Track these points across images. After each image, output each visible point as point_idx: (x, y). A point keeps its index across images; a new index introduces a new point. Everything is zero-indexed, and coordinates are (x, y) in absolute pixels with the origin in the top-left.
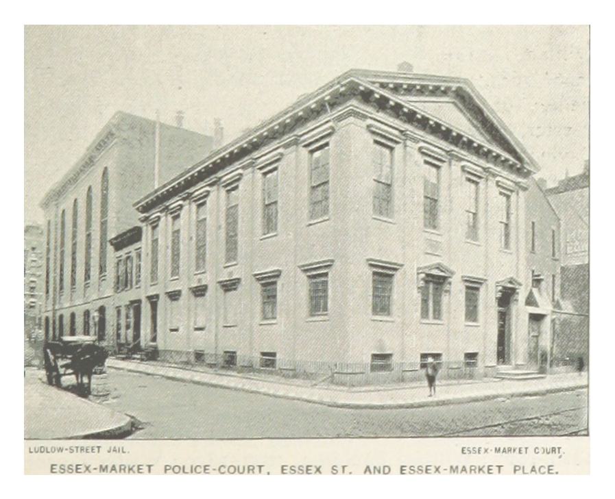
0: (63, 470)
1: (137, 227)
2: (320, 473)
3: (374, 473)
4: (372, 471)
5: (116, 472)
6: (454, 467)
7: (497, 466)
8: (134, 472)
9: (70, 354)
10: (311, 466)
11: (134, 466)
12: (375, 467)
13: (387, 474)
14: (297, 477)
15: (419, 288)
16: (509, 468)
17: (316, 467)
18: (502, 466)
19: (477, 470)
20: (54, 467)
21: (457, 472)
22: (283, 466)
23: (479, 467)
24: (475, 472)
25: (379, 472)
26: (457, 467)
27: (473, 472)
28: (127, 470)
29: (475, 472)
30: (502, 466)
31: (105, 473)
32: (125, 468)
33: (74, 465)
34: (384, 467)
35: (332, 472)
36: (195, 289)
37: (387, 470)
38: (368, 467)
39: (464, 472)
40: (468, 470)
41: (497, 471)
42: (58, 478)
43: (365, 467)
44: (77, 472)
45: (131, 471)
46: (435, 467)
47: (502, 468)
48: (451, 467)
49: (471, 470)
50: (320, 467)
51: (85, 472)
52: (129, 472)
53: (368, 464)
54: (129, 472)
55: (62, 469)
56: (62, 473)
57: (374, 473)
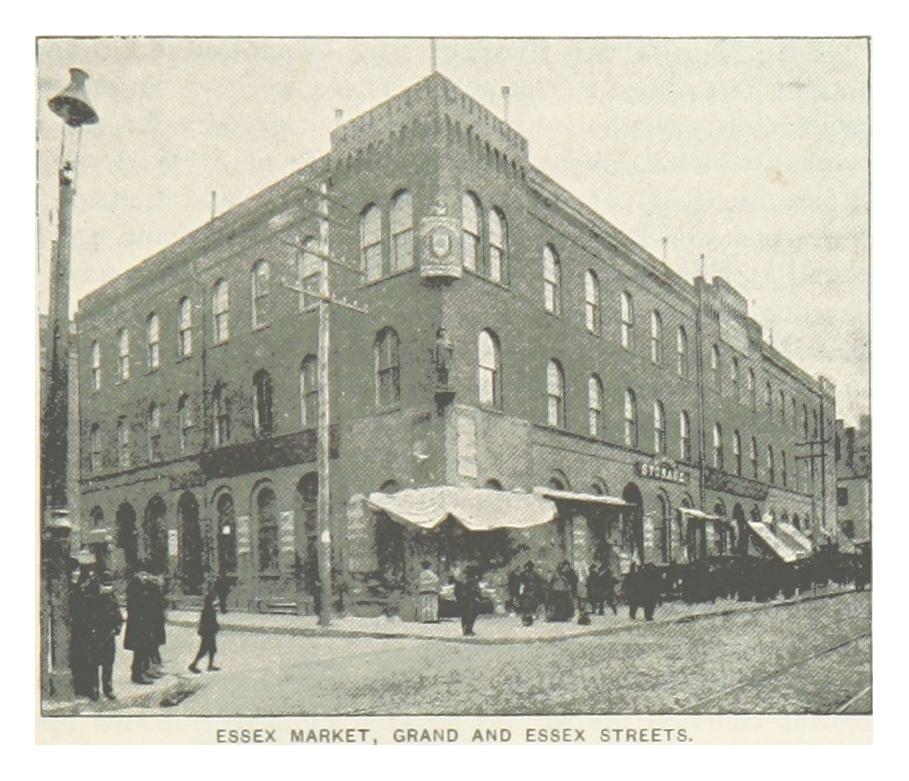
0: (234, 738)
1: (307, 475)
2: (274, 740)
3: (435, 739)
4: (432, 737)
5: (316, 740)
6: (297, 732)
7: (360, 730)
8: (341, 740)
9: (519, 588)
10: (659, 730)
11: (341, 731)
12: (435, 732)
13: (452, 741)
14: (240, 747)
15: (96, 524)
16: (519, 734)
17: (267, 732)
18: (367, 730)
19: (331, 737)
20: (531, 733)
21: (302, 740)
22: (528, 730)
23: (334, 732)
24: (328, 740)
25: (495, 738)
26: (301, 732)
27: (324, 739)
28: (331, 737)
29: (328, 740)
30: (367, 730)
31: (299, 743)
32: (635, 733)
33: (651, 730)
34: (503, 731)
35: (601, 739)
36: (859, 443)
37: (452, 735)
38: (478, 731)
39: (312, 740)
40: (318, 736)
41: (666, 737)
42: (228, 748)
43: (474, 732)
44: (565, 740)
45: (337, 739)
46: (577, 731)
47: (367, 733)
48: (293, 732)
49: (322, 736)
50: (583, 731)
51: (267, 740)
52: (334, 740)
53: (478, 727)
54: (334, 740)
55: (234, 736)
56: (233, 742)
57: (488, 739)
